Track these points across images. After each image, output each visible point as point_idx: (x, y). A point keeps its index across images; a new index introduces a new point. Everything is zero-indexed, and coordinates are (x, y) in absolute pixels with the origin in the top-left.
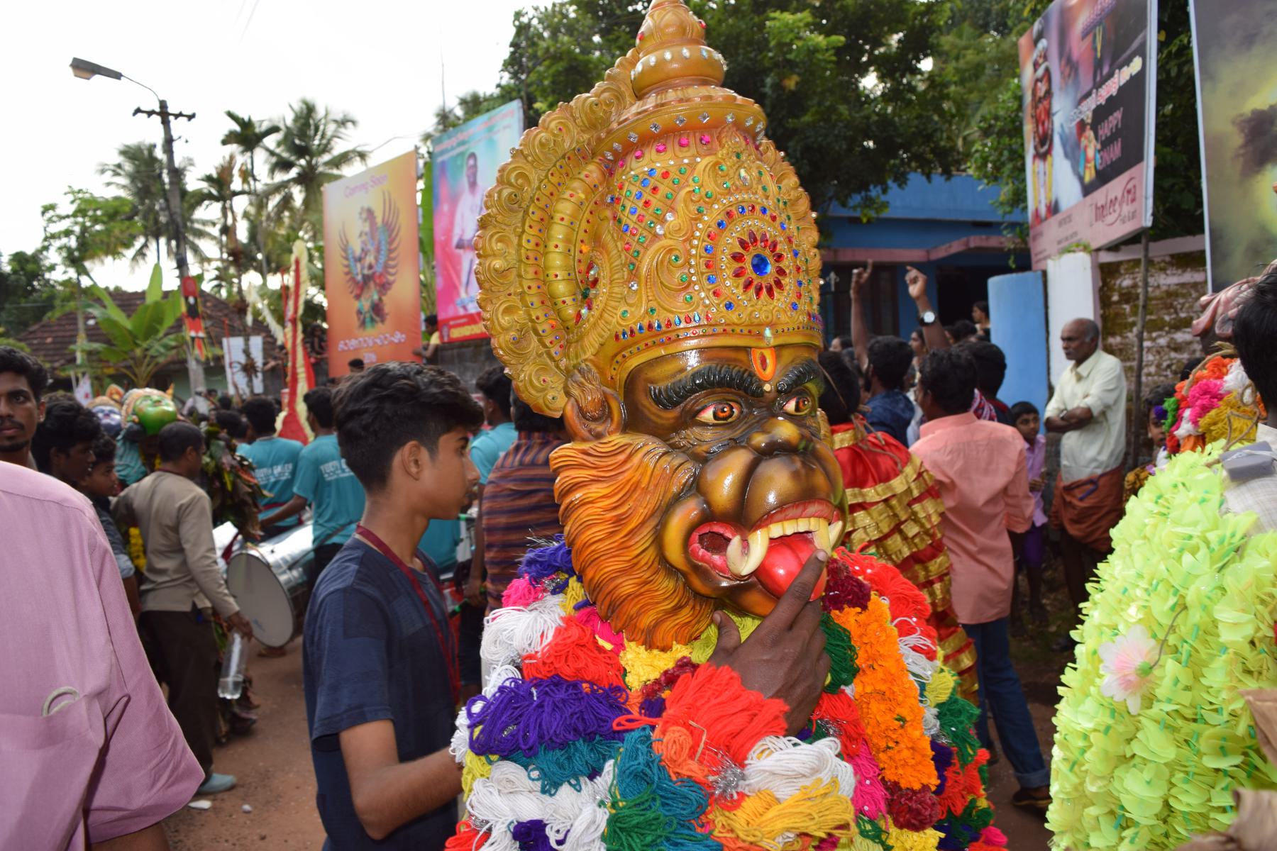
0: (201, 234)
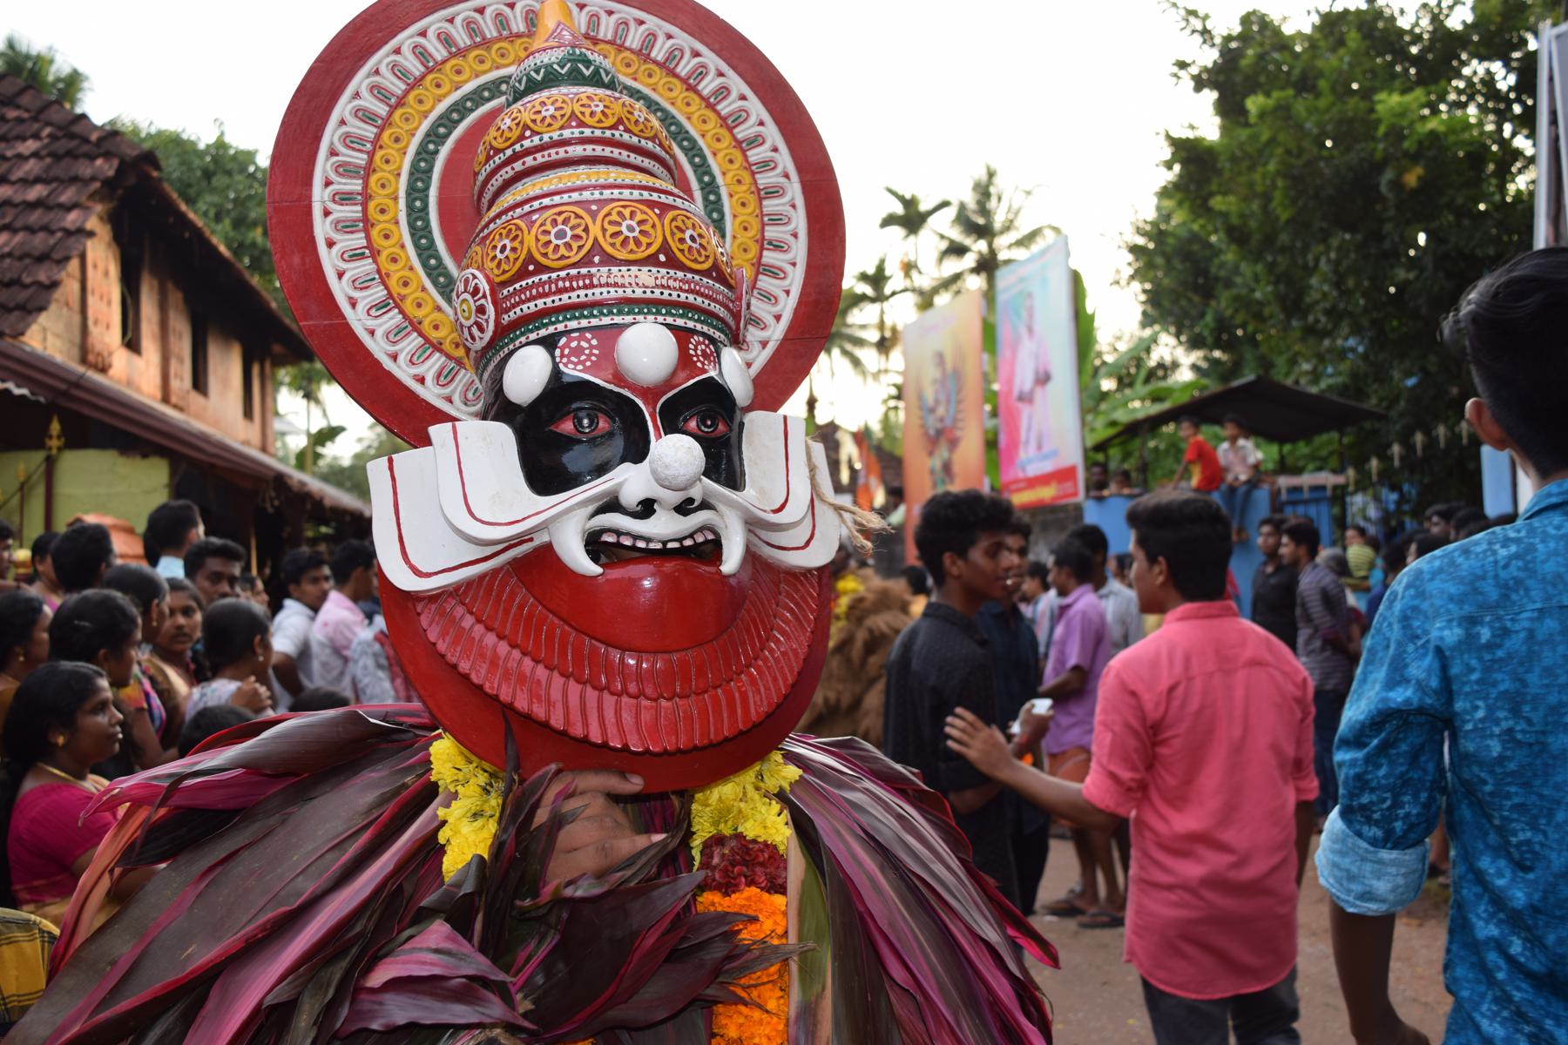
0: (859, 342)
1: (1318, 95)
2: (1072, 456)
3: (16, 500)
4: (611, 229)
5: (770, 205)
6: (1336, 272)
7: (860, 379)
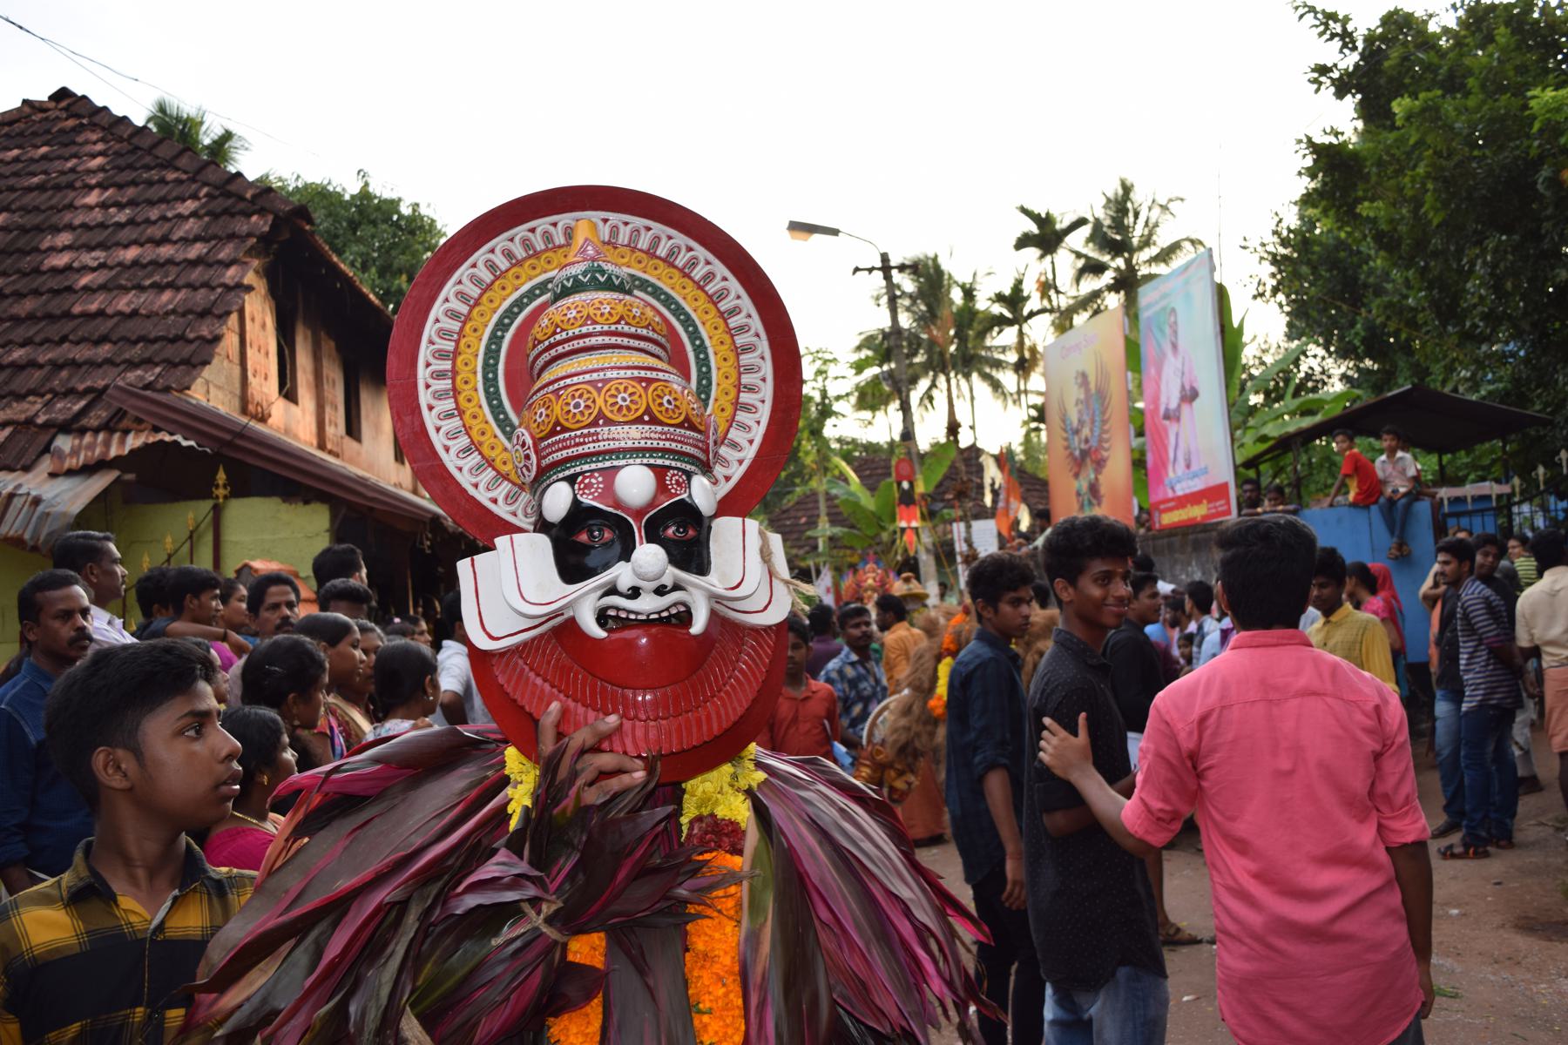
0: (998, 364)
1: (1467, 94)
2: (1223, 473)
3: (187, 546)
4: (611, 401)
5: (746, 359)
6: (1492, 274)
7: (1000, 402)
